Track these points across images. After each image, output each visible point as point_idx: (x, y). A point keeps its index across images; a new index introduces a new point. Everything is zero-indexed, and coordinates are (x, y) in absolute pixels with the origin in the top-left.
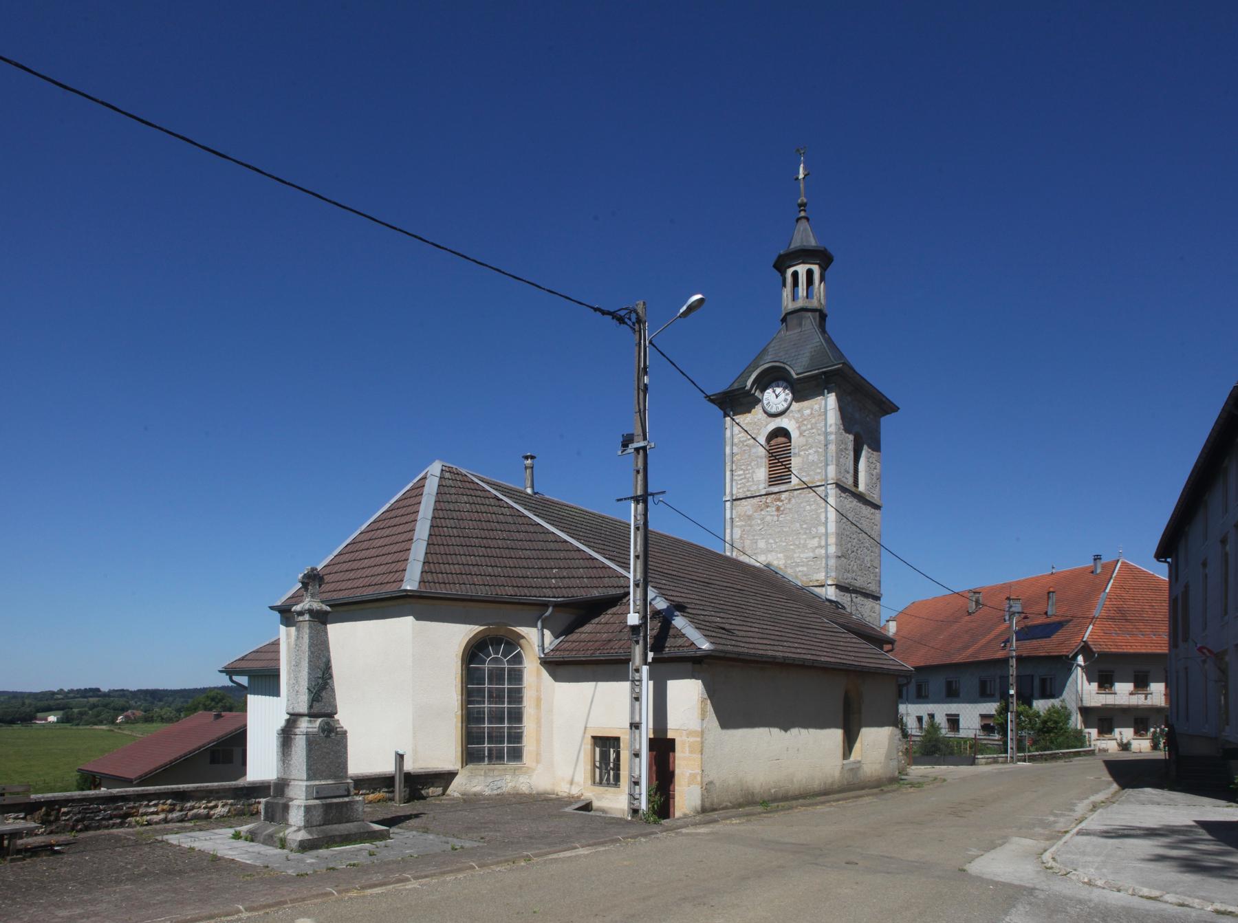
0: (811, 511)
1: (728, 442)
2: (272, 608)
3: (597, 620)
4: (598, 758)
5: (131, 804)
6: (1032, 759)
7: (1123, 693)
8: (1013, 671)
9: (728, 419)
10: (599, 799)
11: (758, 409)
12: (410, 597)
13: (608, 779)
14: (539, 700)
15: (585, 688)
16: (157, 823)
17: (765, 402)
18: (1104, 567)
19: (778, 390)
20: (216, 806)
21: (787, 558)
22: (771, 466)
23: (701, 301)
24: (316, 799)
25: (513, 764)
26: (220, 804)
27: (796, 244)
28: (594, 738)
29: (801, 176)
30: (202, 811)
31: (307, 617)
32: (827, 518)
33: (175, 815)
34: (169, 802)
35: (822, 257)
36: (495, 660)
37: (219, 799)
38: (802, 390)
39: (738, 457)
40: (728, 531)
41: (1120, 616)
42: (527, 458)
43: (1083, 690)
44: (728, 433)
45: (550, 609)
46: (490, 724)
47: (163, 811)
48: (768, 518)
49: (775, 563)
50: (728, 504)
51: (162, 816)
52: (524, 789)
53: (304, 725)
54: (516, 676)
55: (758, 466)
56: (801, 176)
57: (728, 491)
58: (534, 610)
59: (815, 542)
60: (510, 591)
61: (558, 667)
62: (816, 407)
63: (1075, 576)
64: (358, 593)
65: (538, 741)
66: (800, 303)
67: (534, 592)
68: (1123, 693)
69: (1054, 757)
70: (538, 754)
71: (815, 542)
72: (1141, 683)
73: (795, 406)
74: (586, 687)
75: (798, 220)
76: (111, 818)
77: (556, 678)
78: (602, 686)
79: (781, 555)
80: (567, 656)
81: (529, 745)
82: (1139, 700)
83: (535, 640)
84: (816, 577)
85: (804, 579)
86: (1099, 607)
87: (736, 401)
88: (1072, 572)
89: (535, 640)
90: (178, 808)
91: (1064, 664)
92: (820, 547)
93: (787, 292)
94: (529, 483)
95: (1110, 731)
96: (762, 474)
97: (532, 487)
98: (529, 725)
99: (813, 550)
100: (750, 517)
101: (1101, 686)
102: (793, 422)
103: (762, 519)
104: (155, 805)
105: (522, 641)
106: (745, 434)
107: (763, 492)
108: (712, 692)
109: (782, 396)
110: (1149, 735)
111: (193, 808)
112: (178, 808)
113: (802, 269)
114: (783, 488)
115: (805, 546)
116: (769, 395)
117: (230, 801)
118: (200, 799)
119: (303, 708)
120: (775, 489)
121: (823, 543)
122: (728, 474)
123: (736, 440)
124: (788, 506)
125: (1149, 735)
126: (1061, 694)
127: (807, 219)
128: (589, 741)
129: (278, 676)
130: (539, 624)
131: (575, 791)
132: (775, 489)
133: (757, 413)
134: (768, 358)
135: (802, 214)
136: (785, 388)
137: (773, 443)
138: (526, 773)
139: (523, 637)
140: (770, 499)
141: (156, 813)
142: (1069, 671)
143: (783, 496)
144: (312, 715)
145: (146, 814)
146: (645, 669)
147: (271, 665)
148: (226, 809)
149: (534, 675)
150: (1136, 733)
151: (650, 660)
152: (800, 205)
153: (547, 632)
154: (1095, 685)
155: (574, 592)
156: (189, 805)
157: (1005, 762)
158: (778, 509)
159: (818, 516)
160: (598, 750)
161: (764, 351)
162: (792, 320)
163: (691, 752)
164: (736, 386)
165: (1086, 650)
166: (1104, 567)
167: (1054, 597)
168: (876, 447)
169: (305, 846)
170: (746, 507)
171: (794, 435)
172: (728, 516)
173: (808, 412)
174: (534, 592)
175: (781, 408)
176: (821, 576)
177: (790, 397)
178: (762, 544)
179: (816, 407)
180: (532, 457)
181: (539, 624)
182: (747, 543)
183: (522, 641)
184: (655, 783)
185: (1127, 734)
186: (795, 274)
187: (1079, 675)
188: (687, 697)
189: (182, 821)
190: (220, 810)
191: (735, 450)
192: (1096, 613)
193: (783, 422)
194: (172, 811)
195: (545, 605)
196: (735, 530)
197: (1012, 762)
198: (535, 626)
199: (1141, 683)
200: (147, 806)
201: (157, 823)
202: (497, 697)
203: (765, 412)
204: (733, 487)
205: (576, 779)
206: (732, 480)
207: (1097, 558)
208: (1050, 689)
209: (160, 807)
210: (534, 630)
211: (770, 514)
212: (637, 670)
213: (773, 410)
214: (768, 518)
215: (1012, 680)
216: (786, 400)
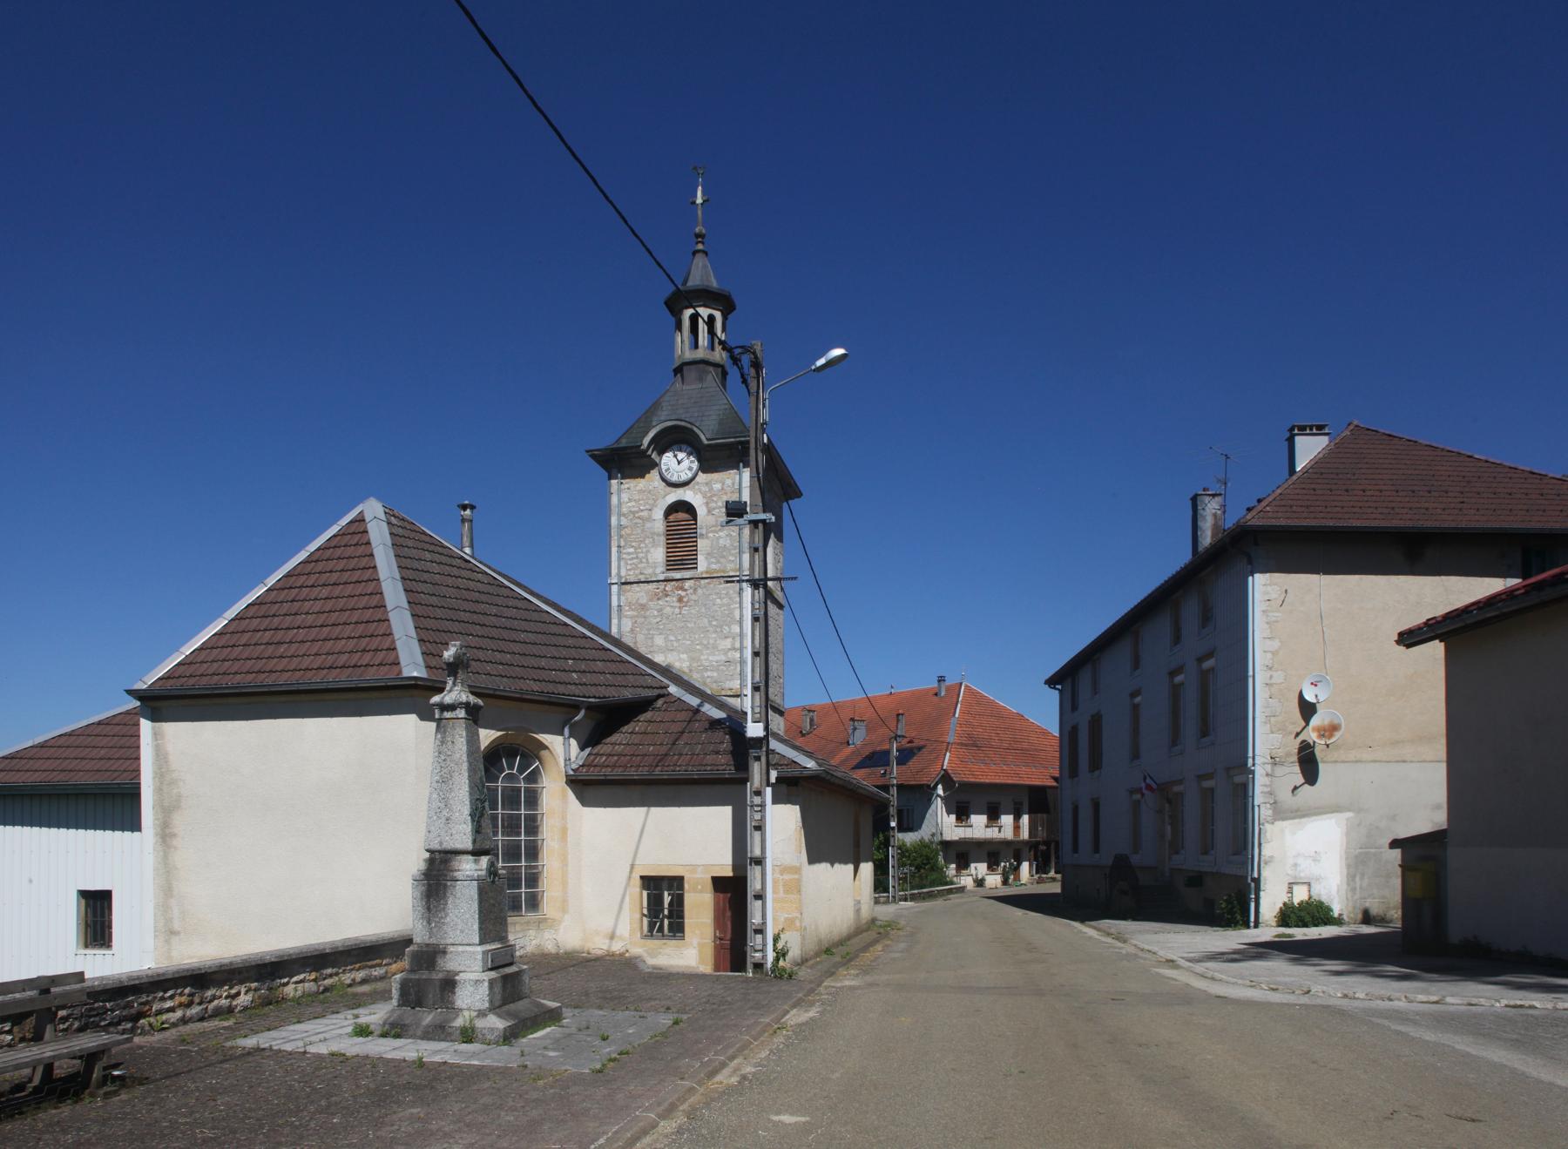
0: (721, 606)
1: (614, 510)
2: (130, 692)
3: (625, 729)
4: (645, 904)
5: (144, 998)
6: (913, 898)
7: (978, 827)
8: (894, 801)
9: (614, 482)
10: (653, 956)
11: (654, 474)
12: (415, 687)
13: (661, 929)
14: (564, 831)
15: (632, 816)
16: (174, 1025)
17: (664, 467)
18: (948, 689)
19: (681, 455)
20: (238, 994)
21: (692, 659)
22: (670, 546)
23: (843, 357)
24: (491, 969)
25: (531, 916)
26: (243, 990)
27: (695, 281)
28: (642, 878)
29: (699, 201)
30: (224, 1002)
31: (461, 713)
32: (741, 616)
33: (195, 1010)
34: (187, 991)
35: (724, 302)
36: (510, 777)
37: (241, 982)
38: (713, 459)
39: (628, 531)
40: (615, 621)
41: (972, 744)
42: (464, 507)
43: (942, 823)
44: (614, 500)
45: (582, 713)
46: (502, 860)
47: (181, 1005)
48: (668, 610)
49: (677, 665)
50: (615, 588)
51: (179, 1014)
52: (550, 947)
53: (469, 868)
54: (533, 799)
55: (654, 545)
56: (699, 201)
57: (614, 571)
58: (559, 712)
59: (727, 643)
60: (536, 687)
61: (588, 787)
62: (729, 482)
63: (917, 697)
64: (270, 680)
65: (564, 884)
66: (700, 354)
67: (561, 689)
68: (978, 827)
69: (930, 896)
70: (565, 901)
71: (727, 643)
72: (993, 816)
73: (702, 477)
74: (634, 815)
75: (695, 253)
76: (119, 1023)
77: (585, 802)
78: (658, 813)
79: (684, 656)
80: (594, 774)
81: (550, 887)
82: (992, 833)
83: (562, 750)
84: (729, 685)
85: (714, 686)
86: (951, 733)
87: (626, 461)
88: (913, 693)
89: (562, 750)
90: (197, 1000)
91: (926, 793)
92: (734, 649)
93: (682, 340)
94: (466, 541)
95: (966, 866)
96: (659, 554)
97: (472, 546)
98: (549, 861)
99: (726, 652)
100: (643, 607)
101: (959, 819)
102: (699, 496)
103: (660, 610)
104: (171, 998)
105: (544, 753)
106: (638, 503)
107: (662, 577)
108: (809, 824)
109: (686, 463)
110: (1000, 870)
111: (214, 998)
112: (197, 1000)
113: (704, 312)
114: (687, 574)
115: (715, 647)
116: (668, 460)
117: (254, 985)
118: (220, 985)
119: (462, 836)
120: (678, 575)
121: (737, 645)
122: (614, 550)
123: (624, 510)
124: (694, 597)
125: (1000, 870)
126: (919, 827)
127: (706, 253)
128: (638, 882)
129: (139, 795)
130: (566, 731)
131: (617, 947)
132: (678, 575)
133: (652, 480)
134: (663, 414)
135: (700, 247)
136: (689, 454)
137: (671, 518)
138: (551, 927)
139: (546, 748)
140: (669, 587)
141: (172, 1010)
142: (929, 803)
143: (687, 584)
144: (477, 853)
145: (160, 1012)
146: (769, 790)
147: (124, 779)
148: (249, 997)
149: (555, 796)
150: (989, 868)
151: (773, 780)
152: (698, 236)
153: (573, 742)
154: (953, 817)
155: (602, 691)
156: (209, 993)
157: (887, 902)
158: (680, 600)
159: (731, 612)
160: (645, 893)
161: (655, 406)
162: (690, 373)
163: (786, 892)
164: (624, 443)
165: (946, 779)
166: (948, 689)
167: (903, 720)
168: (780, 538)
169: (509, 1036)
170: (639, 593)
171: (701, 512)
172: (615, 603)
173: (717, 486)
174: (192, 681)
175: (684, 477)
176: (736, 684)
177: (695, 465)
178: (659, 641)
179: (729, 482)
180: (472, 507)
181: (566, 731)
182: (640, 638)
183: (544, 753)
184: (268, 959)
185: (980, 869)
186: (694, 319)
187: (938, 806)
188: (783, 825)
189: (202, 1019)
190: (244, 999)
191: (624, 521)
192: (951, 738)
193: (687, 495)
194: (189, 1005)
195: (576, 707)
196: (624, 621)
197: (894, 901)
198: (561, 734)
199: (993, 816)
200: (163, 999)
201: (174, 1025)
202: (512, 826)
203: (664, 479)
204: (618, 568)
205: (618, 933)
206: (619, 559)
207: (941, 679)
208: (910, 822)
209: (178, 1000)
210: (560, 738)
211: (670, 605)
212: (758, 793)
213: (674, 479)
214: (668, 610)
215: (893, 811)
216: (690, 469)
